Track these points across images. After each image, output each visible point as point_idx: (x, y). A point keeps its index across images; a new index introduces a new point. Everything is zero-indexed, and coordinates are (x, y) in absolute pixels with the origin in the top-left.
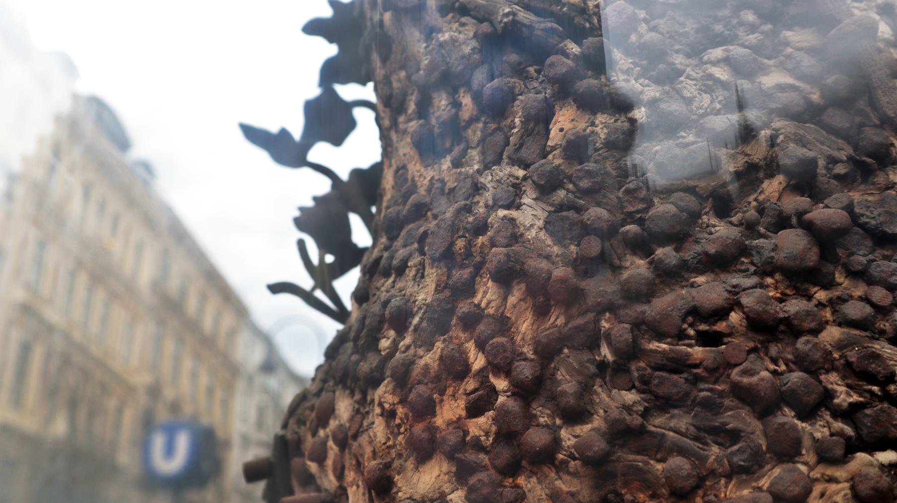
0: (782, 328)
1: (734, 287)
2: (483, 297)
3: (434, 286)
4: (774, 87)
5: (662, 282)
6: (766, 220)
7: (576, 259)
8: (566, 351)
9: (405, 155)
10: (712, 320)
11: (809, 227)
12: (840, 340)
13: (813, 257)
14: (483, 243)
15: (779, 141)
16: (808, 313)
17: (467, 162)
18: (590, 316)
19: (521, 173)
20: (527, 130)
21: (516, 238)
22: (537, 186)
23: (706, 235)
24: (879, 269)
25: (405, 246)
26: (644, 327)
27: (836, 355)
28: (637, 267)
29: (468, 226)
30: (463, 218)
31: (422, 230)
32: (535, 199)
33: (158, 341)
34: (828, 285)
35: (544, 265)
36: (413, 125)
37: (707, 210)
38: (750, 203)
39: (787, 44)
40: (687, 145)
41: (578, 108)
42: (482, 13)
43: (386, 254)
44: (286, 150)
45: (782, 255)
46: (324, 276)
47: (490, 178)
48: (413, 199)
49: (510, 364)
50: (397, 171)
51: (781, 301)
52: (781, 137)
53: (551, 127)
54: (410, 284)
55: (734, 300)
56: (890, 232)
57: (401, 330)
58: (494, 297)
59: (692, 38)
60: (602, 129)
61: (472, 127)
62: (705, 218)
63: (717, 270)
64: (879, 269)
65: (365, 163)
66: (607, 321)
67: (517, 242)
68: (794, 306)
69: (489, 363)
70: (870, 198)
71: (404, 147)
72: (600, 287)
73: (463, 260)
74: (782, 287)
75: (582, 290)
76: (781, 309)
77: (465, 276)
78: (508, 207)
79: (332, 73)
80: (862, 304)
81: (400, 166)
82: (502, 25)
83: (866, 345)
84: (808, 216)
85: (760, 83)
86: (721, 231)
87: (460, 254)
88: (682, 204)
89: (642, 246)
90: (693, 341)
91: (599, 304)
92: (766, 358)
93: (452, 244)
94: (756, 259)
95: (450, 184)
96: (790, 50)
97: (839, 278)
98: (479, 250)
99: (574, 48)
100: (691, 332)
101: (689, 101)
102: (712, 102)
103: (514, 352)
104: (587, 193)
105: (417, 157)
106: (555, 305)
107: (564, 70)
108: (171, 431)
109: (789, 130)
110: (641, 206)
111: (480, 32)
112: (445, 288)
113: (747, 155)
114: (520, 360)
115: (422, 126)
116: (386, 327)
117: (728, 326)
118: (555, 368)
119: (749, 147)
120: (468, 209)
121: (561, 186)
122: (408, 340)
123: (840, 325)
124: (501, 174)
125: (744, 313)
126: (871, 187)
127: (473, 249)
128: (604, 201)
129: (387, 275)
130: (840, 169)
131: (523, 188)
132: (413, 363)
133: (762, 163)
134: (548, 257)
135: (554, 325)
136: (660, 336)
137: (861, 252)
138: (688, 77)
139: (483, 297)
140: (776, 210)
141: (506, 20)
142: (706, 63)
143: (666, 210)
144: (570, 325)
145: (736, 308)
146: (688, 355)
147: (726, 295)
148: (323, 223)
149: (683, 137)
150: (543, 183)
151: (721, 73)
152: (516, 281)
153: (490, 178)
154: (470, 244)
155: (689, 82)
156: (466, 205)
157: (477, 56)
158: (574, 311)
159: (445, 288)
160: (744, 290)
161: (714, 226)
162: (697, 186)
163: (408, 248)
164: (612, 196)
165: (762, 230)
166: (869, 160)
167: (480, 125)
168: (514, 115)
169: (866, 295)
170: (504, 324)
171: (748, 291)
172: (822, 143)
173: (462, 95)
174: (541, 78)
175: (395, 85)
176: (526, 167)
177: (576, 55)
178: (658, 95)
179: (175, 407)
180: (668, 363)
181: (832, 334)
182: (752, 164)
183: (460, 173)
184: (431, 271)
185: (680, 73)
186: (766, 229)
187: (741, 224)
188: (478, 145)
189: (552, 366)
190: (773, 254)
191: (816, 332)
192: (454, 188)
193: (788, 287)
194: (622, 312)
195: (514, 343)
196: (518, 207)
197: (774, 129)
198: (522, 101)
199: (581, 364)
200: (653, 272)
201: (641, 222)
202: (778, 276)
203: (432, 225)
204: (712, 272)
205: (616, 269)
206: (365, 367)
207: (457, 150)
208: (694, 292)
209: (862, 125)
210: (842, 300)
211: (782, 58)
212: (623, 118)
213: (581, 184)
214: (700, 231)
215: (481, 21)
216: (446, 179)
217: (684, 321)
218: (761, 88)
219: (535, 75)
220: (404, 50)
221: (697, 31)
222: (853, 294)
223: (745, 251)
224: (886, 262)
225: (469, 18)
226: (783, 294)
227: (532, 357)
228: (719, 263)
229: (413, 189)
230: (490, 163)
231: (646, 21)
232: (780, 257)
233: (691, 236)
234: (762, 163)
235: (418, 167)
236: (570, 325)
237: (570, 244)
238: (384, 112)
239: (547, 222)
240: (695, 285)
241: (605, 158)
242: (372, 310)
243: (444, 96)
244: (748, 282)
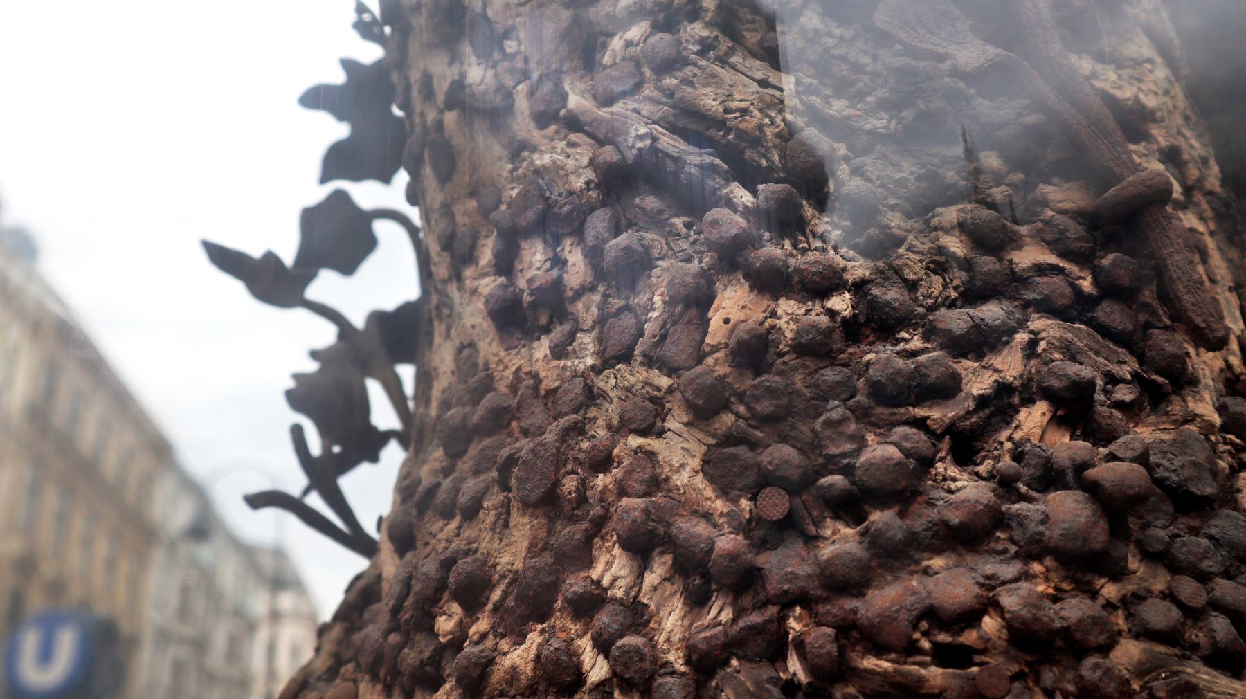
0: (1059, 643)
1: (988, 577)
2: (605, 570)
3: (525, 544)
4: (1030, 269)
5: (880, 566)
6: (1028, 472)
7: (749, 521)
8: (734, 662)
9: (473, 327)
10: (956, 627)
11: (1093, 490)
12: (1140, 663)
13: (1100, 535)
14: (605, 487)
15: (1039, 349)
16: (1095, 621)
17: (574, 351)
18: (772, 610)
19: (665, 382)
20: (672, 315)
21: (656, 484)
22: (690, 406)
23: (943, 494)
24: (1185, 549)
25: (477, 473)
26: (855, 634)
27: (1136, 686)
28: (840, 541)
29: (581, 456)
30: (573, 443)
31: (505, 453)
32: (686, 424)
33: (34, 491)
34: (1118, 573)
35: (701, 529)
36: (489, 285)
37: (943, 454)
38: (1001, 443)
39: (1045, 203)
40: (913, 354)
41: (752, 288)
42: (604, 131)
43: (447, 483)
44: (273, 282)
45: (1057, 532)
46: (323, 474)
47: (613, 381)
48: (488, 400)
49: (651, 678)
50: (460, 350)
51: (1055, 599)
52: (1043, 344)
53: (710, 314)
54: (487, 536)
55: (989, 598)
56: (1199, 493)
57: (472, 605)
58: (623, 573)
59: (912, 188)
60: (787, 322)
61: (583, 299)
62: (940, 467)
63: (960, 549)
64: (1185, 549)
65: (390, 303)
66: (797, 619)
67: (659, 489)
68: (1074, 609)
69: (614, 673)
70: (1165, 437)
71: (472, 314)
72: (786, 565)
73: (574, 509)
74: (1054, 577)
75: (760, 569)
76: (1057, 613)
77: (578, 536)
78: (643, 433)
79: (339, 162)
80: (1167, 604)
81: (465, 343)
82: (634, 152)
83: (1175, 668)
84: (1091, 473)
85: (1011, 261)
86: (966, 489)
87: (570, 501)
88: (908, 445)
89: (849, 507)
90: (928, 659)
91: (786, 592)
92: (1036, 689)
93: (557, 483)
94: (1017, 534)
95: (549, 382)
98: (598, 495)
99: (743, 196)
100: (926, 645)
101: (912, 286)
102: (945, 286)
103: (655, 660)
104: (767, 421)
105: (492, 332)
106: (718, 591)
107: (734, 232)
108: (49, 626)
109: (1052, 333)
110: (848, 447)
111: (601, 159)
112: (544, 549)
113: (996, 371)
114: (666, 674)
115: (504, 287)
116: (446, 596)
117: (981, 638)
118: (717, 687)
119: (1000, 359)
120: (578, 429)
121: (726, 407)
123: (1137, 637)
124: (632, 379)
125: (1003, 618)
126: (1164, 419)
127: (589, 493)
128: (793, 434)
129: (447, 515)
130: (1124, 394)
131: (668, 406)
132: (491, 662)
133: (1017, 383)
134: (707, 516)
135: (715, 623)
136: (880, 650)
137: (1159, 523)
138: (910, 249)
139: (605, 570)
140: (1040, 457)
141: (640, 145)
142: (936, 229)
143: (886, 454)
144: (741, 624)
145: (990, 610)
146: (921, 680)
147: (976, 590)
148: (332, 411)
149: (906, 341)
150: (700, 402)
151: (955, 245)
152: (658, 550)
153: (613, 381)
154: (584, 485)
155: (912, 256)
156: (576, 423)
157: (593, 194)
158: (747, 601)
159: (544, 549)
160: (1004, 583)
161: (954, 480)
162: (928, 417)
163: (482, 477)
164: (805, 429)
165: (1023, 488)
166: (1160, 379)
167: (597, 298)
168: (652, 289)
169: (1169, 588)
170: (637, 616)
171: (1009, 586)
172: (1097, 353)
173: (567, 248)
174: (693, 237)
175: (461, 219)
176: (671, 371)
177: (746, 207)
178: (868, 274)
179: (56, 588)
180: (891, 691)
181: (1129, 652)
182: (1004, 384)
183: (564, 368)
184: (521, 520)
185: (899, 242)
186: (1027, 485)
187: (990, 477)
188: (593, 328)
189: (714, 684)
190: (1041, 528)
191: (1105, 649)
192: (555, 390)
193: (1064, 579)
194: (821, 609)
195: (654, 647)
196: (660, 434)
197: (1031, 332)
198: (664, 270)
199: (758, 684)
200: (867, 549)
201: (847, 471)
202: (1049, 561)
203: (525, 446)
204: (954, 551)
205: (812, 540)
206: (410, 657)
207: (559, 332)
208: (930, 583)
209: (1148, 326)
210: (1140, 597)
211: (1040, 225)
212: (818, 308)
213: (759, 408)
214: (932, 486)
215: (601, 143)
216: (542, 375)
217: (915, 627)
218: (1012, 271)
219: (684, 230)
220: (474, 170)
221: (919, 178)
222: (1153, 588)
223: (999, 520)
224: (1193, 538)
225: (581, 135)
226: (1056, 588)
227: (683, 669)
228: (966, 537)
229: (488, 385)
230: (613, 357)
231: (846, 159)
232: (1053, 534)
233: (921, 494)
234: (1017, 383)
235: (495, 347)
236: (741, 624)
237: (740, 496)
238: (439, 255)
239: (705, 461)
240: (930, 572)
241: (795, 369)
242: (423, 570)
243: (540, 246)
244: (1009, 570)
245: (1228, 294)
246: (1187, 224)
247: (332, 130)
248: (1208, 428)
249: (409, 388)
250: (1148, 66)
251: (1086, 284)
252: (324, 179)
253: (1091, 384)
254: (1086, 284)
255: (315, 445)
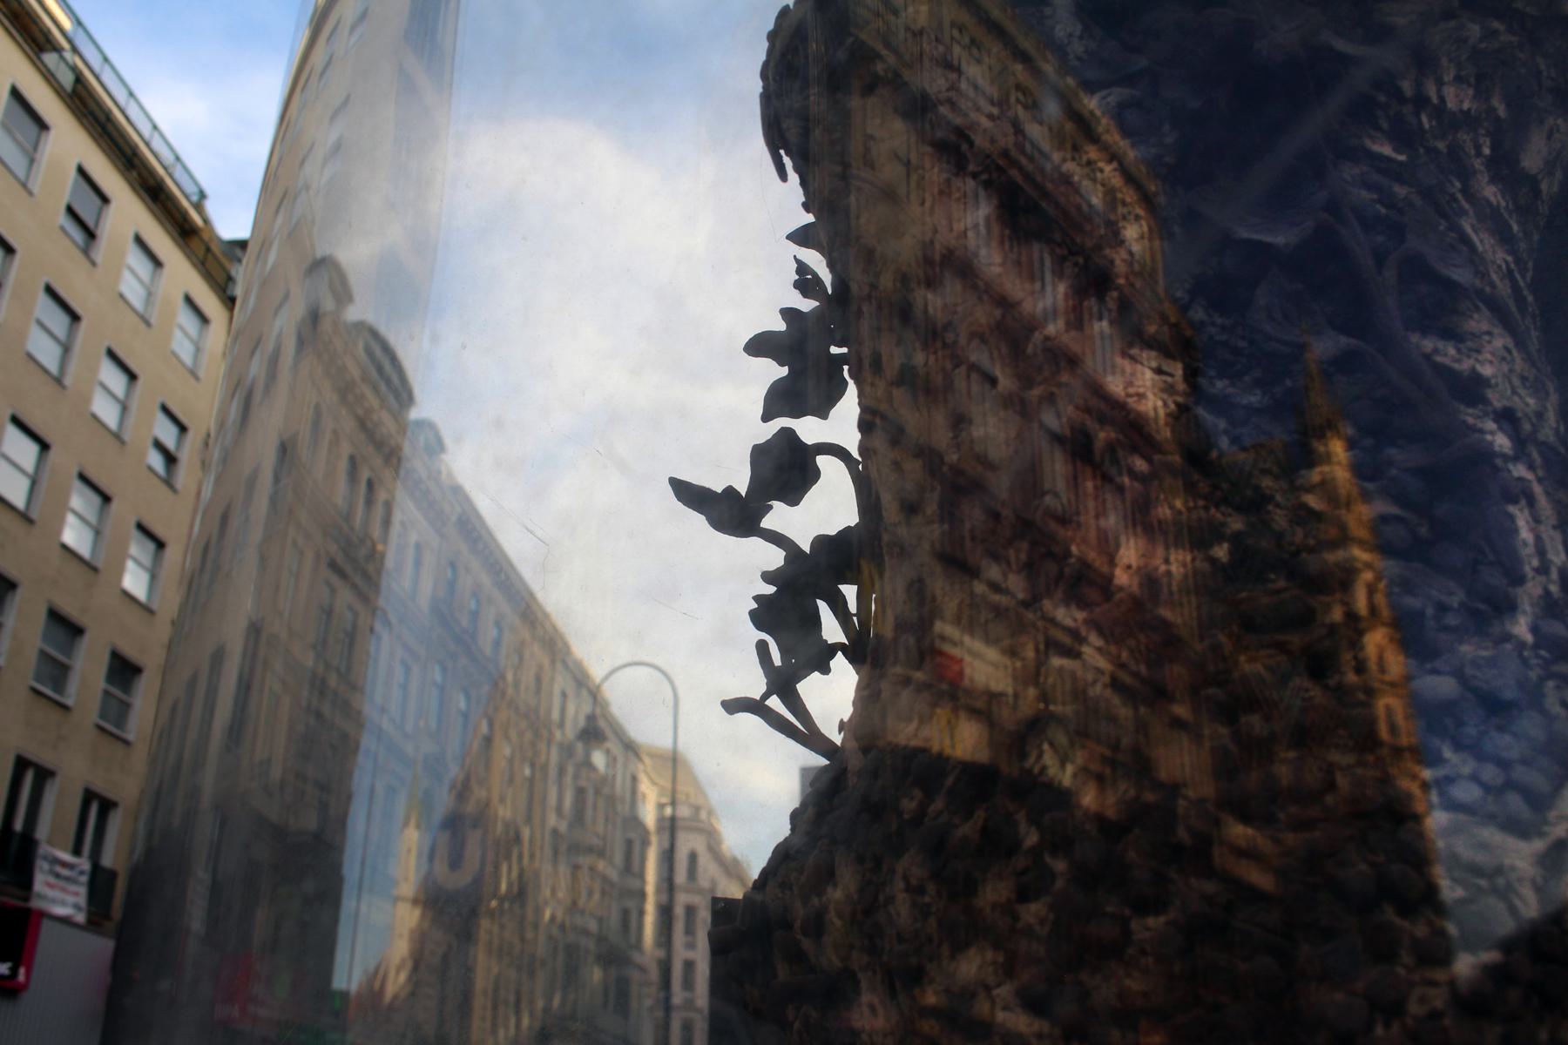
40: (1278, 592)
44: (734, 514)
46: (783, 683)
79: (781, 400)
96: (1394, 472)
97: (1448, 753)
101: (1279, 536)
102: (1306, 536)
122: (938, 804)
148: (786, 610)
231: (1226, 432)
245: (1551, 532)
246: (1516, 474)
247: (771, 371)
248: (1522, 645)
249: (853, 606)
250: (1487, 338)
251: (1423, 531)
252: (766, 418)
253: (1420, 614)
254: (1423, 531)
255: (777, 660)
